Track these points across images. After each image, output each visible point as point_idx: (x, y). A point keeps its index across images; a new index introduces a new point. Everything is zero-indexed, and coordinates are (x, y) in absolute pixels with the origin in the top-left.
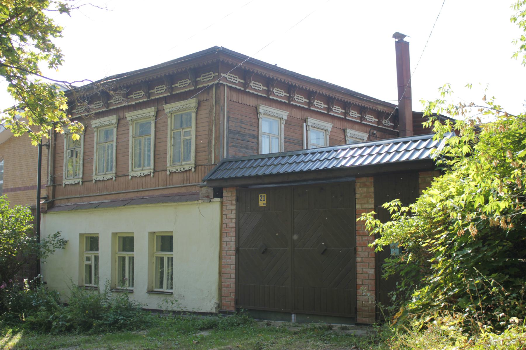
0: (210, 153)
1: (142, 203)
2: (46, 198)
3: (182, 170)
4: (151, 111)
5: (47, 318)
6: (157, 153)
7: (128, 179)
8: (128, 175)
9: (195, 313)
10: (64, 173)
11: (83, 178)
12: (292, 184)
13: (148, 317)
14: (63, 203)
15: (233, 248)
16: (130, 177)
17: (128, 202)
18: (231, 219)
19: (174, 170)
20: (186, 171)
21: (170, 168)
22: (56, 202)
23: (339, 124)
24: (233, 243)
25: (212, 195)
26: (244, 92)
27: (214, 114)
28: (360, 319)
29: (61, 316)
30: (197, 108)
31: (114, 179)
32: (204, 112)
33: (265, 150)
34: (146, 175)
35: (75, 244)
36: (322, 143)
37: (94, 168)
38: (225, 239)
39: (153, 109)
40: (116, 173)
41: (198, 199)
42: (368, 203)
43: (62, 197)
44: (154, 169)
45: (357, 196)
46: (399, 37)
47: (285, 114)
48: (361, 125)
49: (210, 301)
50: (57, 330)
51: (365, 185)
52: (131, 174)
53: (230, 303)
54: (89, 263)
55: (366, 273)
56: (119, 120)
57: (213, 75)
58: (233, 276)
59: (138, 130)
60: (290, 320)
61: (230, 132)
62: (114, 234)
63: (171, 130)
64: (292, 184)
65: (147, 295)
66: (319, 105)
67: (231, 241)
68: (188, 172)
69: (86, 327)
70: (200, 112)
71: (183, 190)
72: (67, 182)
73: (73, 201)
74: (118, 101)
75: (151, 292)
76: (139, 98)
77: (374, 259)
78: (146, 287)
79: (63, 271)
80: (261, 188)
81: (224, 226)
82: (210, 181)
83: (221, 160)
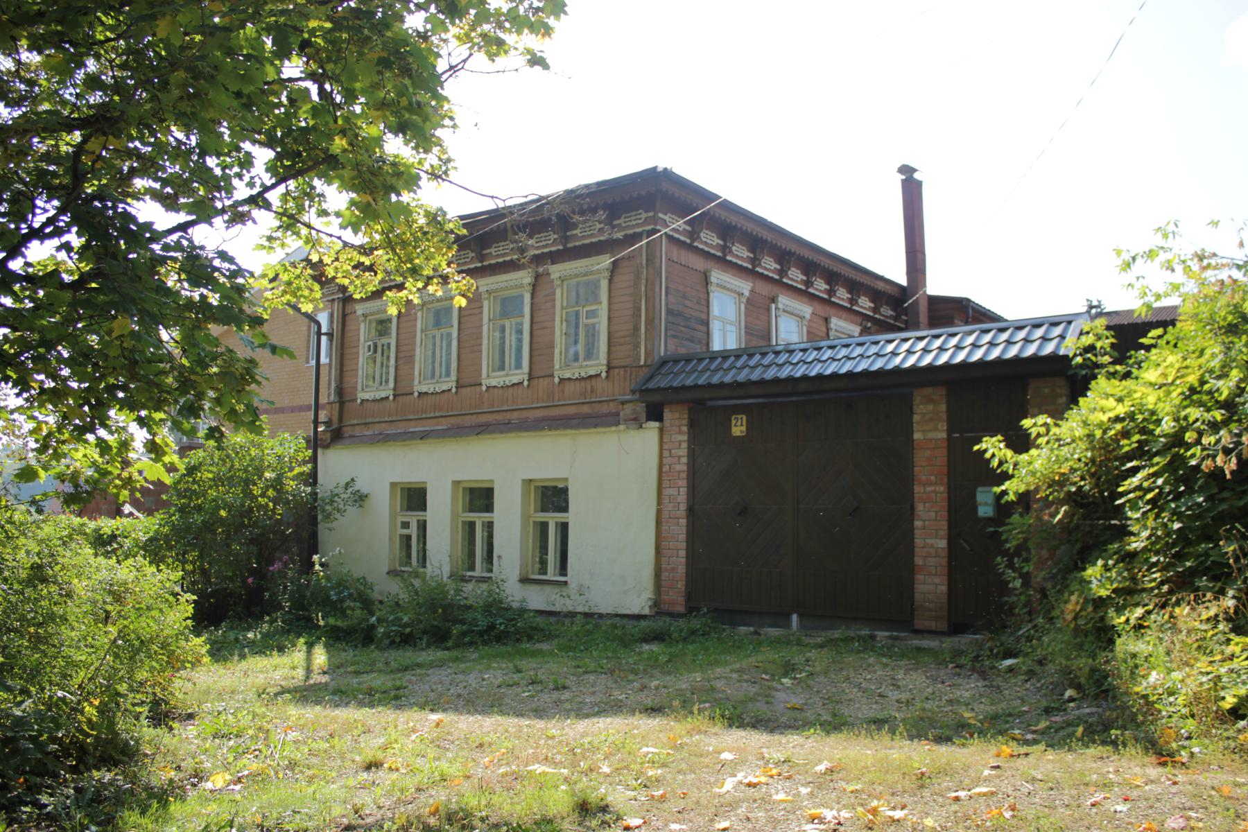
0: (637, 346)
1: (511, 430)
2: (328, 424)
3: (583, 374)
4: (524, 277)
5: (367, 620)
6: (534, 346)
7: (481, 393)
9: (617, 615)
10: (360, 381)
11: (395, 389)
12: (794, 399)
13: (540, 620)
14: (357, 431)
15: (683, 507)
16: (484, 388)
17: (482, 429)
18: (679, 457)
19: (567, 375)
20: (591, 377)
21: (559, 372)
22: (345, 429)
23: (822, 310)
24: (682, 497)
25: (644, 416)
26: (690, 248)
27: (644, 281)
28: (918, 624)
29: (391, 618)
30: (612, 272)
31: (454, 390)
32: (623, 279)
33: (716, 346)
34: (514, 385)
35: (382, 502)
36: (794, 338)
37: (417, 373)
38: (667, 492)
40: (457, 381)
41: (617, 424)
42: (935, 429)
43: (355, 422)
44: (530, 374)
45: (916, 418)
46: (907, 171)
47: (745, 286)
48: (849, 312)
49: (639, 596)
50: (387, 642)
51: (929, 400)
52: (486, 382)
53: (676, 599)
54: (406, 532)
55: (932, 546)
56: (537, 277)
57: (644, 215)
58: (683, 553)
59: (498, 308)
60: (788, 625)
61: (669, 312)
62: (456, 483)
63: (562, 308)
64: (794, 399)
65: (519, 585)
66: (795, 276)
67: (679, 494)
68: (593, 380)
69: (439, 637)
70: (616, 279)
71: (586, 409)
72: (366, 396)
73: (376, 429)
74: (589, 230)
75: (525, 580)
76: (592, 236)
77: (945, 523)
78: (518, 572)
79: (360, 546)
80: (736, 405)
81: (666, 468)
82: (644, 392)
83: (656, 358)
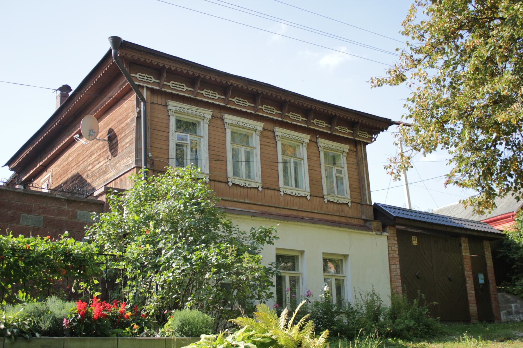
8: (279, 191)
39: (309, 137)
